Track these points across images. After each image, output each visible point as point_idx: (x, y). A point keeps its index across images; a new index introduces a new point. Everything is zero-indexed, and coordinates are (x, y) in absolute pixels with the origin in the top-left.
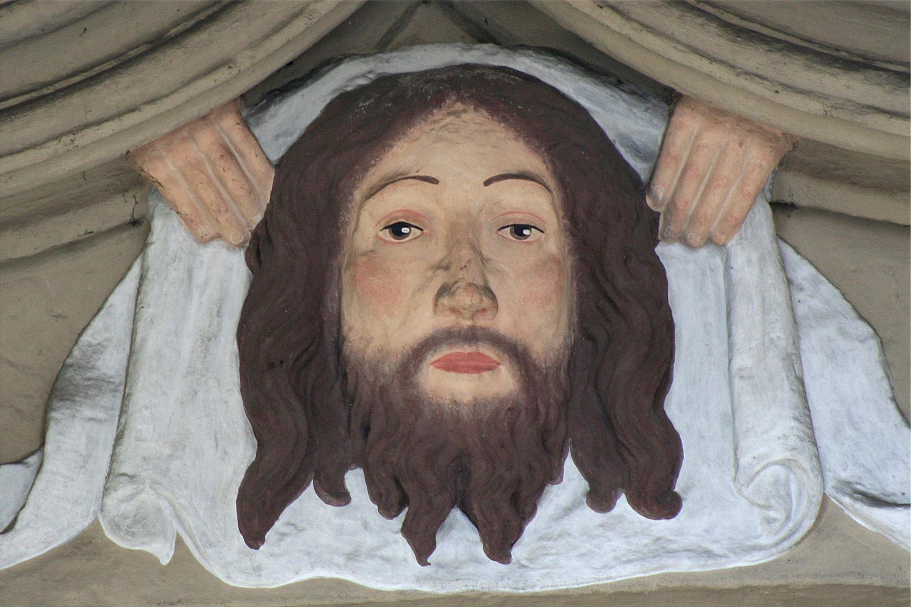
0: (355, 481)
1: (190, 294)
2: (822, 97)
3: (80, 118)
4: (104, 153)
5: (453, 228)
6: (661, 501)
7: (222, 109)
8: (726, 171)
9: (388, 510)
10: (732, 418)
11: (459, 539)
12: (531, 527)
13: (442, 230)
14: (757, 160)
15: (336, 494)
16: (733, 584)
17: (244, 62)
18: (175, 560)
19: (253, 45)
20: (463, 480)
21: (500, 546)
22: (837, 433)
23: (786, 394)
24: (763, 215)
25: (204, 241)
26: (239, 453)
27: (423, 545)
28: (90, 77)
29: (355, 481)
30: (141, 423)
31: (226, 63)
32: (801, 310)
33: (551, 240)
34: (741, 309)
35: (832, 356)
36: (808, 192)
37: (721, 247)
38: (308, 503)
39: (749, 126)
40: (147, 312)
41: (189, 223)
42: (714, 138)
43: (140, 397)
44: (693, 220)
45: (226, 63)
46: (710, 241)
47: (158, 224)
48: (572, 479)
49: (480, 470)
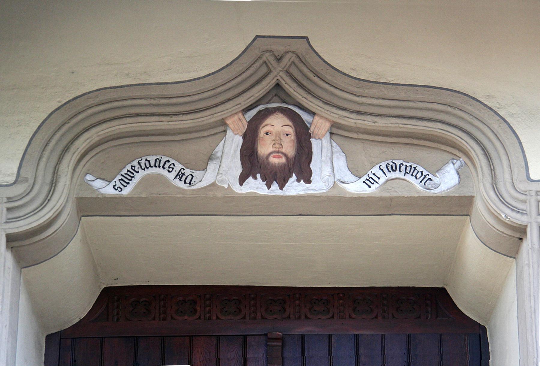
0: (258, 176)
1: (232, 143)
2: (338, 115)
3: (215, 112)
4: (221, 118)
5: (276, 133)
6: (308, 181)
7: (239, 112)
8: (322, 127)
9: (263, 181)
10: (321, 168)
11: (275, 186)
12: (286, 185)
13: (274, 134)
14: (327, 125)
15: (255, 178)
16: (319, 195)
17: (243, 104)
18: (272, 183)
19: (245, 101)
20: (277, 176)
21: (281, 188)
22: (338, 171)
23: (330, 164)
24: (328, 135)
25: (235, 134)
26: (240, 170)
27: (269, 187)
28: (217, 105)
29: (258, 176)
30: (223, 165)
31: (240, 104)
32: (333, 151)
33: (293, 137)
34: (323, 150)
35: (338, 158)
36: (336, 131)
37: (321, 139)
38: (251, 178)
39: (327, 119)
40: (225, 146)
41: (233, 131)
42: (321, 121)
43: (223, 160)
44: (316, 135)
45: (240, 104)
46: (319, 138)
47: (228, 131)
48: (294, 177)
49: (279, 175)
